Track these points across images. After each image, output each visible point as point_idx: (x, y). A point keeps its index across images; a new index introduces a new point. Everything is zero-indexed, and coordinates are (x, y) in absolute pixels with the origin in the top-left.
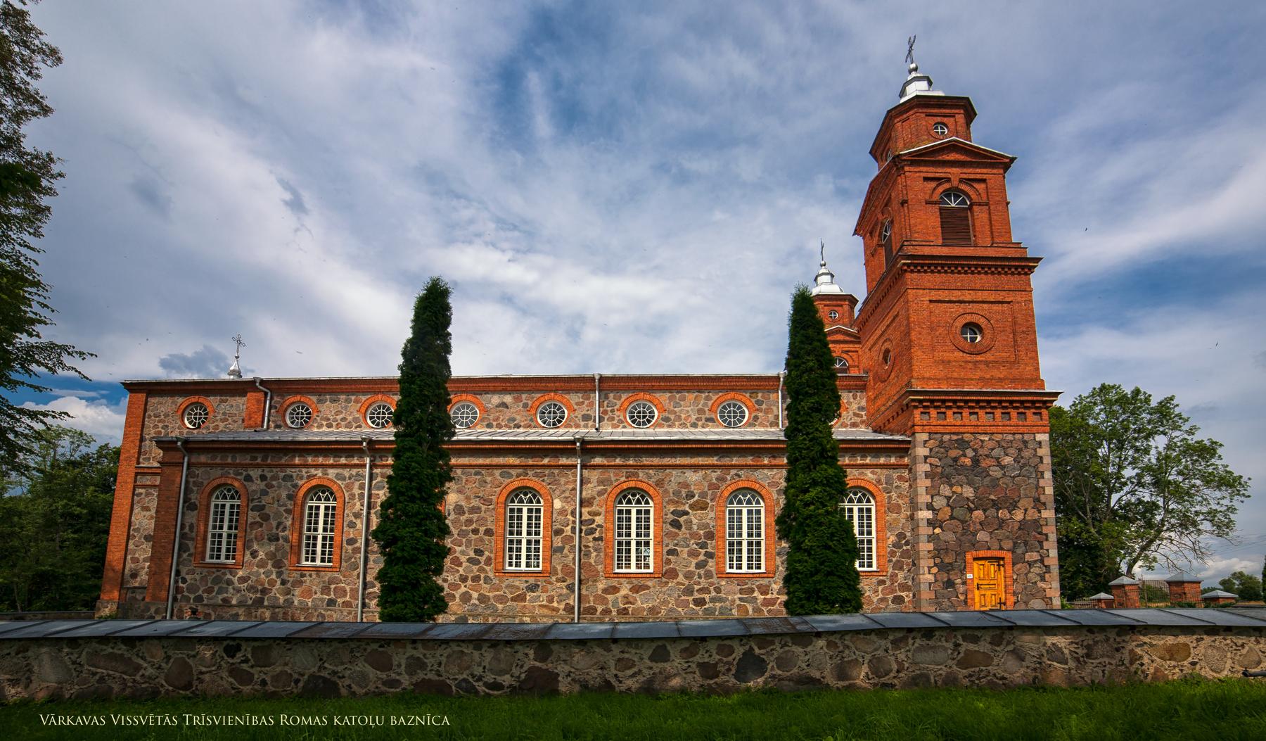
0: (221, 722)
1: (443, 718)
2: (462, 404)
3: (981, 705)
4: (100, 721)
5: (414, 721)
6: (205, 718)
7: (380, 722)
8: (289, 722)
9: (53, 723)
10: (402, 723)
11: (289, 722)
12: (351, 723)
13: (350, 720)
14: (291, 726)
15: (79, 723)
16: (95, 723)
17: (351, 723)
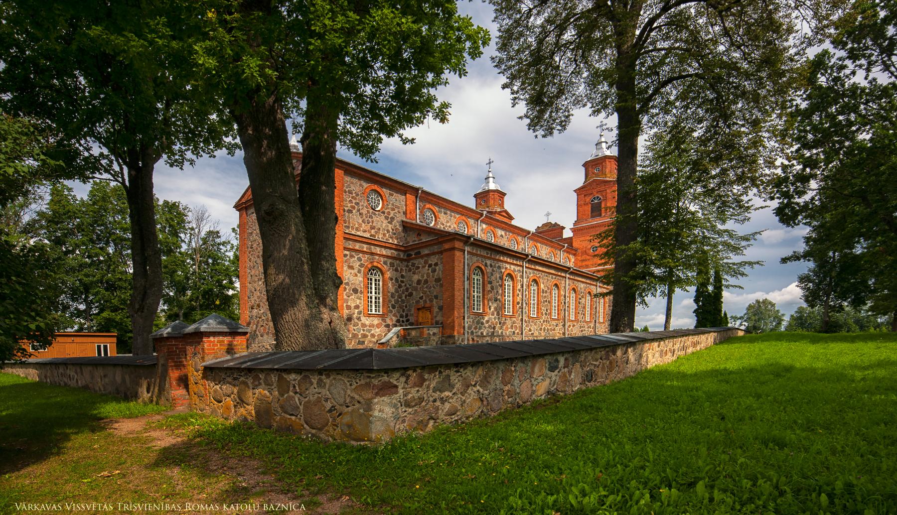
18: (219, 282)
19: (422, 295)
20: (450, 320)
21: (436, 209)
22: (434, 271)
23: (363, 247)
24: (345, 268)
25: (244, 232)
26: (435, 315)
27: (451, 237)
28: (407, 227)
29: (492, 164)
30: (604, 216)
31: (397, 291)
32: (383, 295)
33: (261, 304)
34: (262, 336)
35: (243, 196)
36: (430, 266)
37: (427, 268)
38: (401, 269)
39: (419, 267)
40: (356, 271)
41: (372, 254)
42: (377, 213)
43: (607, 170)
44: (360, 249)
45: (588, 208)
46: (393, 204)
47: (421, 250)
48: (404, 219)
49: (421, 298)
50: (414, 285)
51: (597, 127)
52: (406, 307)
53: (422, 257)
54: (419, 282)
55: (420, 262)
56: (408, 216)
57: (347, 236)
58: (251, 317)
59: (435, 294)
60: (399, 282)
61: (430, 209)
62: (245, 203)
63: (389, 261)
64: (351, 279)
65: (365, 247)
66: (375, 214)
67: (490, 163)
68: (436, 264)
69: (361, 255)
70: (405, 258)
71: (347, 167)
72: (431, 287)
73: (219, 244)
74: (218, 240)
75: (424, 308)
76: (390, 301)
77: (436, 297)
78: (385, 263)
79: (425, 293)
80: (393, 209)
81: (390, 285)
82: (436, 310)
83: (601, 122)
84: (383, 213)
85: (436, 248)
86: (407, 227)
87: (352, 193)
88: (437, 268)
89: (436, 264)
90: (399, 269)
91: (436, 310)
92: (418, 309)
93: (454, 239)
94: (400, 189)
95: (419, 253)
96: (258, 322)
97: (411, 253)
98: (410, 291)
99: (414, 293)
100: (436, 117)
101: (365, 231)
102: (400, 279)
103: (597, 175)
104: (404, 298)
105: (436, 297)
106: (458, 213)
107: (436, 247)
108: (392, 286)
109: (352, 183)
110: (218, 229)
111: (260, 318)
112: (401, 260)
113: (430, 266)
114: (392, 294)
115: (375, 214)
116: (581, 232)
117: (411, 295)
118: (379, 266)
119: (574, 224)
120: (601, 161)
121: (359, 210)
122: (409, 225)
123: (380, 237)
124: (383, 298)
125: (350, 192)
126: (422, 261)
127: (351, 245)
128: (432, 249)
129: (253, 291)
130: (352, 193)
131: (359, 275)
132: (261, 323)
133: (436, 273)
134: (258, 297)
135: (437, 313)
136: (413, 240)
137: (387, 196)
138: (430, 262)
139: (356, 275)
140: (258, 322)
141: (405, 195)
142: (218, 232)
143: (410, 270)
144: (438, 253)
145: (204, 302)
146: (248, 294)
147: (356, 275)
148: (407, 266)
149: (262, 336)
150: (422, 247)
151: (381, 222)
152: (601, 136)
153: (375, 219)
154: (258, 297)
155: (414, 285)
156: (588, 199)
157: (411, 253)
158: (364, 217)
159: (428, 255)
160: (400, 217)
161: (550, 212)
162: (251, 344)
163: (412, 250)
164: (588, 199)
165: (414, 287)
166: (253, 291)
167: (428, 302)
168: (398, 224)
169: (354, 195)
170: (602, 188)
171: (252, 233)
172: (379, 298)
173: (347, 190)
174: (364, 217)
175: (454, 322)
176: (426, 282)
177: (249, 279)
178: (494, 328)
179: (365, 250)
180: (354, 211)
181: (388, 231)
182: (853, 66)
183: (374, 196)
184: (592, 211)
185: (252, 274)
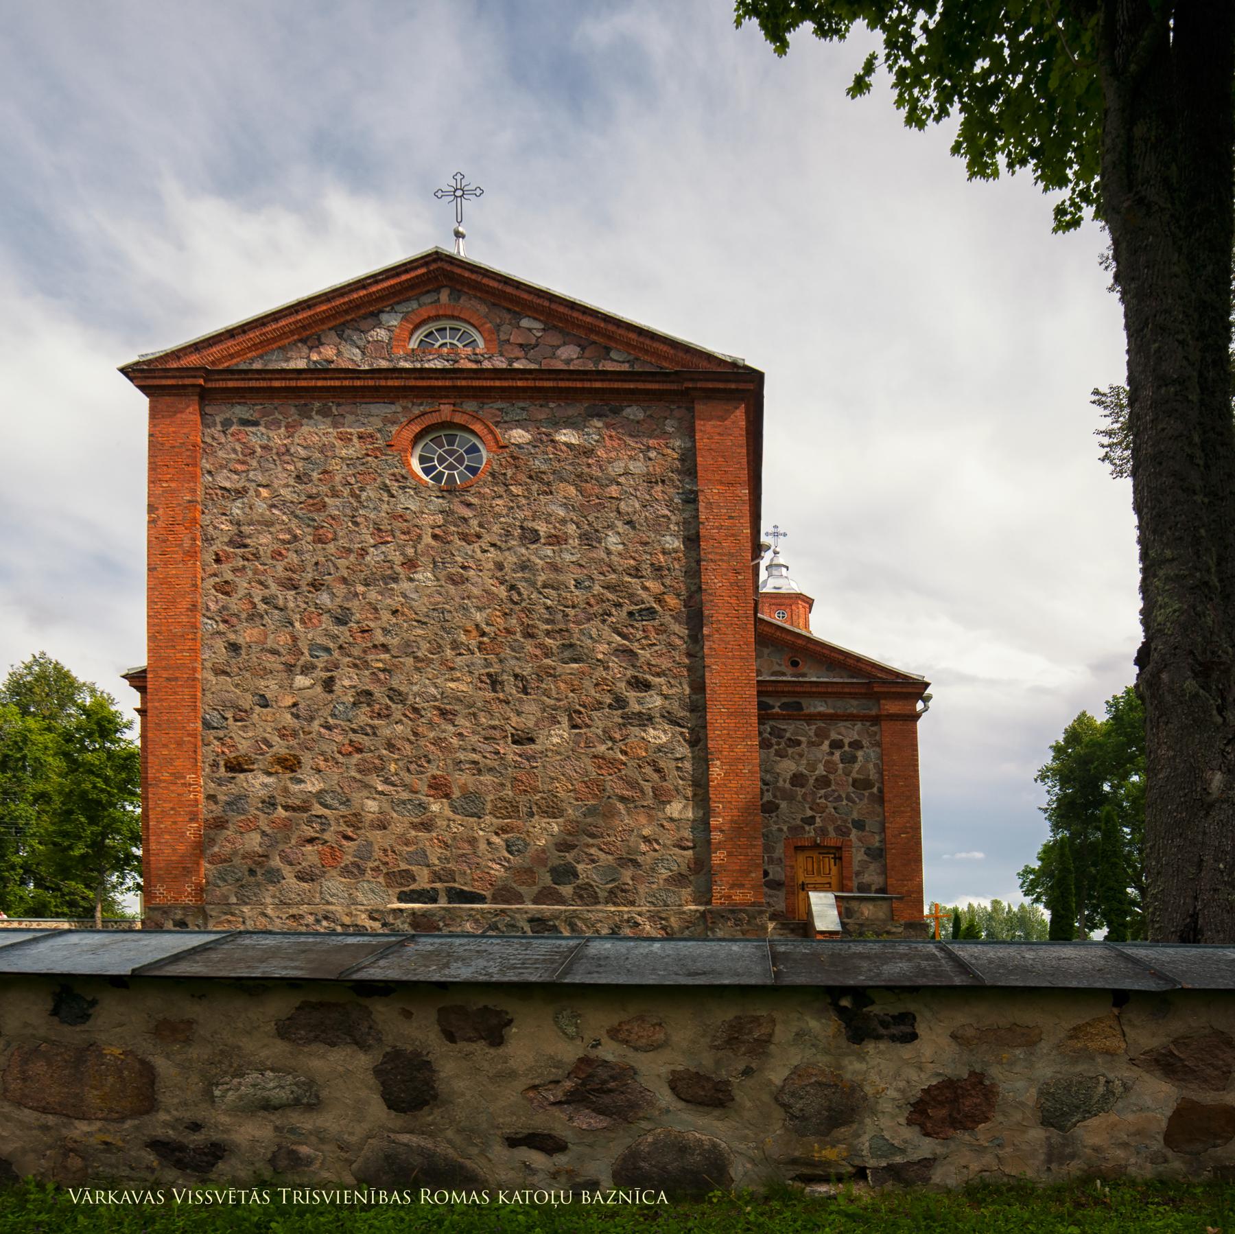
0: (186, 1198)
1: (657, 1194)
2: (440, 324)
3: (1135, 778)
4: (402, 1198)
5: (616, 1199)
6: (311, 1195)
7: (566, 1198)
8: (433, 1200)
9: (87, 1201)
10: (598, 1201)
11: (433, 1200)
12: (524, 1200)
13: (523, 1196)
14: (436, 1205)
15: (126, 1201)
16: (149, 1201)
17: (524, 1200)
19: (809, 813)
22: (850, 759)
26: (856, 868)
35: (197, 347)
36: (836, 745)
37: (826, 746)
47: (804, 702)
49: (810, 821)
51: (785, 535)
53: (810, 718)
54: (798, 779)
59: (855, 816)
62: (208, 373)
72: (839, 798)
77: (859, 825)
85: (853, 707)
88: (860, 754)
89: (856, 745)
91: (858, 856)
95: (799, 706)
99: (783, 805)
105: (859, 825)
107: (854, 702)
128: (839, 703)
133: (857, 766)
135: (864, 865)
138: (834, 736)
144: (863, 718)
150: (811, 695)
165: (783, 790)
167: (832, 834)
176: (824, 782)
182: (453, 653)
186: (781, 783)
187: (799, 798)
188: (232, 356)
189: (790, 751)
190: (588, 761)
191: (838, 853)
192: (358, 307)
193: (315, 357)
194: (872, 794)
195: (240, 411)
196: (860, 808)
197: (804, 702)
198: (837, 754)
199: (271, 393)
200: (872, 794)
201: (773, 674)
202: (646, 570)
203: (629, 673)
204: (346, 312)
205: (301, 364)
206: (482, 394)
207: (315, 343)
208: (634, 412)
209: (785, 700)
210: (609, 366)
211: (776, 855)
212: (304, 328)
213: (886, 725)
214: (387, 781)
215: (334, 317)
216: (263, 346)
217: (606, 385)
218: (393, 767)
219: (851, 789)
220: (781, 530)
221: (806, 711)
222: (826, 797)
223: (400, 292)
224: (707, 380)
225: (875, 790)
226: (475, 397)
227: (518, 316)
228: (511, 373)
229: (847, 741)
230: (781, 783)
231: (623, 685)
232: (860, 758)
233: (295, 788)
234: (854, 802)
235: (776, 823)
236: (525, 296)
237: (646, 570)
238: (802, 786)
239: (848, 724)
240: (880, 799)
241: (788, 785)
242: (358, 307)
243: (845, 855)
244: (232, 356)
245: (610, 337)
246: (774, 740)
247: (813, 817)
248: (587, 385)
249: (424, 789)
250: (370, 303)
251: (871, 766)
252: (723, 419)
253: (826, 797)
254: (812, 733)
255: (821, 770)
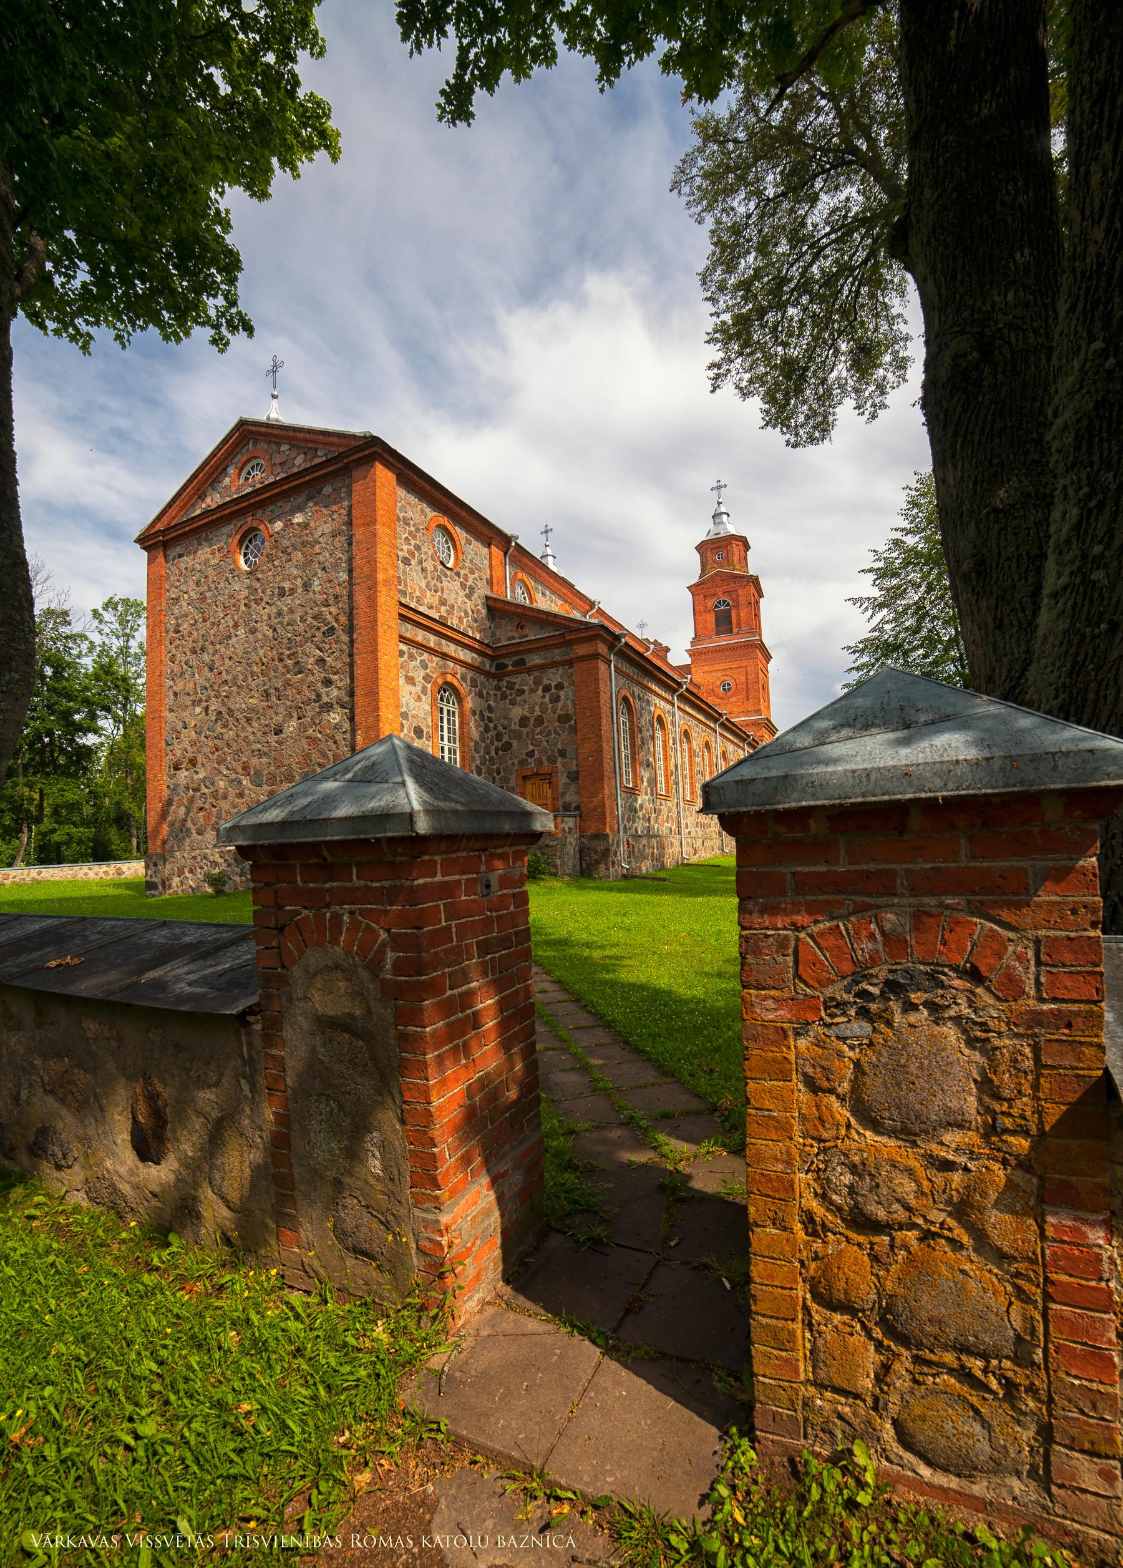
18: (66, 715)
19: (531, 748)
20: (595, 800)
21: (531, 583)
22: (555, 699)
23: (429, 640)
24: (402, 681)
25: (160, 596)
26: (561, 790)
27: (590, 633)
28: (496, 609)
29: (549, 534)
30: (738, 633)
31: (483, 740)
32: (462, 745)
33: (200, 759)
34: (200, 832)
35: (159, 518)
36: (547, 689)
37: (540, 692)
38: (488, 693)
39: (522, 692)
40: (418, 689)
41: (445, 656)
42: (448, 573)
43: (735, 559)
44: (424, 643)
45: (711, 618)
46: (471, 561)
47: (526, 657)
48: (489, 594)
49: (531, 754)
50: (515, 727)
51: (725, 486)
52: (499, 773)
53: (529, 671)
54: (524, 721)
55: (524, 681)
56: (495, 588)
57: (405, 612)
58: (174, 789)
59: (559, 746)
60: (486, 718)
61: (522, 581)
62: (163, 532)
63: (470, 674)
64: (411, 706)
65: (432, 640)
66: (446, 576)
67: (546, 532)
68: (560, 687)
69: (426, 656)
70: (493, 671)
71: (402, 467)
72: (549, 733)
73: (67, 638)
74: (65, 630)
75: (536, 774)
76: (473, 759)
77: (563, 753)
78: (463, 678)
79: (538, 744)
80: (472, 572)
81: (472, 724)
82: (562, 779)
83: (718, 481)
84: (458, 574)
85: (557, 655)
86: (496, 609)
87: (408, 524)
88: (562, 693)
89: (560, 687)
90: (485, 692)
91: (562, 779)
92: (524, 778)
93: (597, 637)
94: (482, 534)
95: (522, 662)
96: (192, 800)
97: (506, 661)
98: (505, 738)
99: (515, 743)
100: (137, 604)
101: (430, 607)
102: (487, 714)
103: (720, 565)
104: (493, 754)
105: (563, 753)
106: (560, 597)
107: (557, 651)
108: (476, 728)
109: (410, 504)
110: (66, 607)
111: (196, 790)
112: (488, 674)
113: (547, 689)
114: (476, 743)
115: (446, 576)
116: (703, 657)
117: (507, 747)
118: (456, 683)
119: (693, 643)
120: (724, 544)
121: (420, 562)
122: (499, 606)
123: (453, 622)
124: (462, 752)
125: (406, 522)
126: (530, 679)
127: (410, 631)
129: (179, 726)
130: (408, 524)
131: (423, 698)
132: (200, 803)
133: (560, 704)
134: (193, 743)
136: (507, 635)
137: (463, 542)
138: (546, 682)
139: (419, 699)
140: (192, 800)
141: (489, 547)
142: (65, 614)
143: (504, 697)
144: (563, 663)
145: (32, 759)
146: (166, 735)
147: (419, 699)
148: (498, 688)
149: (200, 832)
150: (529, 651)
151: (453, 591)
152: (719, 503)
153: (445, 584)
154: (193, 743)
155: (515, 727)
156: (711, 603)
157: (506, 661)
158: (429, 578)
159: (542, 667)
160: (483, 590)
161: (645, 621)
162: (172, 851)
163: (509, 655)
164: (711, 603)
165: (514, 731)
166: (179, 726)
167: (546, 763)
168: (479, 602)
169: (412, 529)
170: (731, 587)
171: (178, 599)
172: (455, 751)
173: (401, 515)
174: (429, 578)
175: (604, 806)
176: (539, 721)
177: (169, 700)
178: (649, 820)
179: (432, 645)
180: (413, 562)
181: (466, 612)
183: (441, 539)
184: (717, 625)
185: (177, 689)
186: (513, 727)
187: (524, 736)
188: (174, 518)
189: (518, 699)
190: (304, 741)
191: (549, 778)
192: (217, 468)
193: (204, 506)
194: (570, 726)
195: (178, 550)
196: (562, 740)
197: (526, 657)
198: (547, 696)
199: (186, 535)
200: (570, 726)
201: (509, 639)
202: (331, 601)
203: (323, 675)
204: (213, 473)
205: (198, 512)
206: (261, 505)
207: (202, 497)
208: (327, 490)
209: (514, 659)
210: (317, 461)
211: (511, 785)
212: (198, 490)
213: (577, 666)
214: (228, 769)
215: (208, 478)
216: (189, 504)
217: (311, 477)
218: (229, 758)
219: (557, 724)
220: (722, 483)
221: (528, 665)
222: (541, 733)
223: (232, 451)
224: (354, 454)
225: (572, 722)
226: (261, 507)
227: (279, 444)
228: (276, 482)
229: (553, 685)
230: (513, 727)
231: (319, 685)
232: (562, 697)
233: (196, 777)
234: (559, 734)
235: (511, 758)
236: (276, 432)
237: (331, 601)
238: (526, 727)
239: (553, 670)
240: (574, 730)
241: (517, 727)
242: (217, 468)
243: (554, 779)
244: (174, 518)
245: (315, 442)
246: (508, 693)
247: (533, 751)
248: (303, 480)
249: (240, 770)
250: (221, 463)
251: (569, 702)
252: (365, 478)
253: (541, 733)
254: (531, 682)
255: (538, 712)
